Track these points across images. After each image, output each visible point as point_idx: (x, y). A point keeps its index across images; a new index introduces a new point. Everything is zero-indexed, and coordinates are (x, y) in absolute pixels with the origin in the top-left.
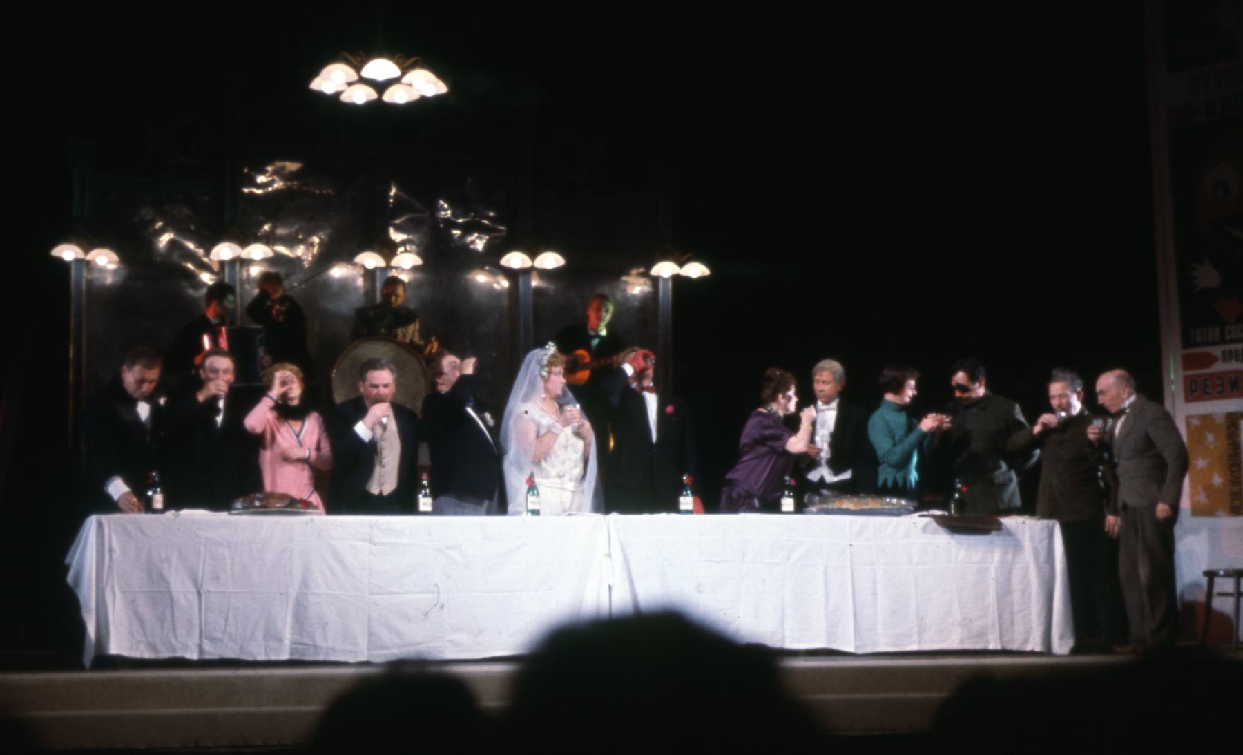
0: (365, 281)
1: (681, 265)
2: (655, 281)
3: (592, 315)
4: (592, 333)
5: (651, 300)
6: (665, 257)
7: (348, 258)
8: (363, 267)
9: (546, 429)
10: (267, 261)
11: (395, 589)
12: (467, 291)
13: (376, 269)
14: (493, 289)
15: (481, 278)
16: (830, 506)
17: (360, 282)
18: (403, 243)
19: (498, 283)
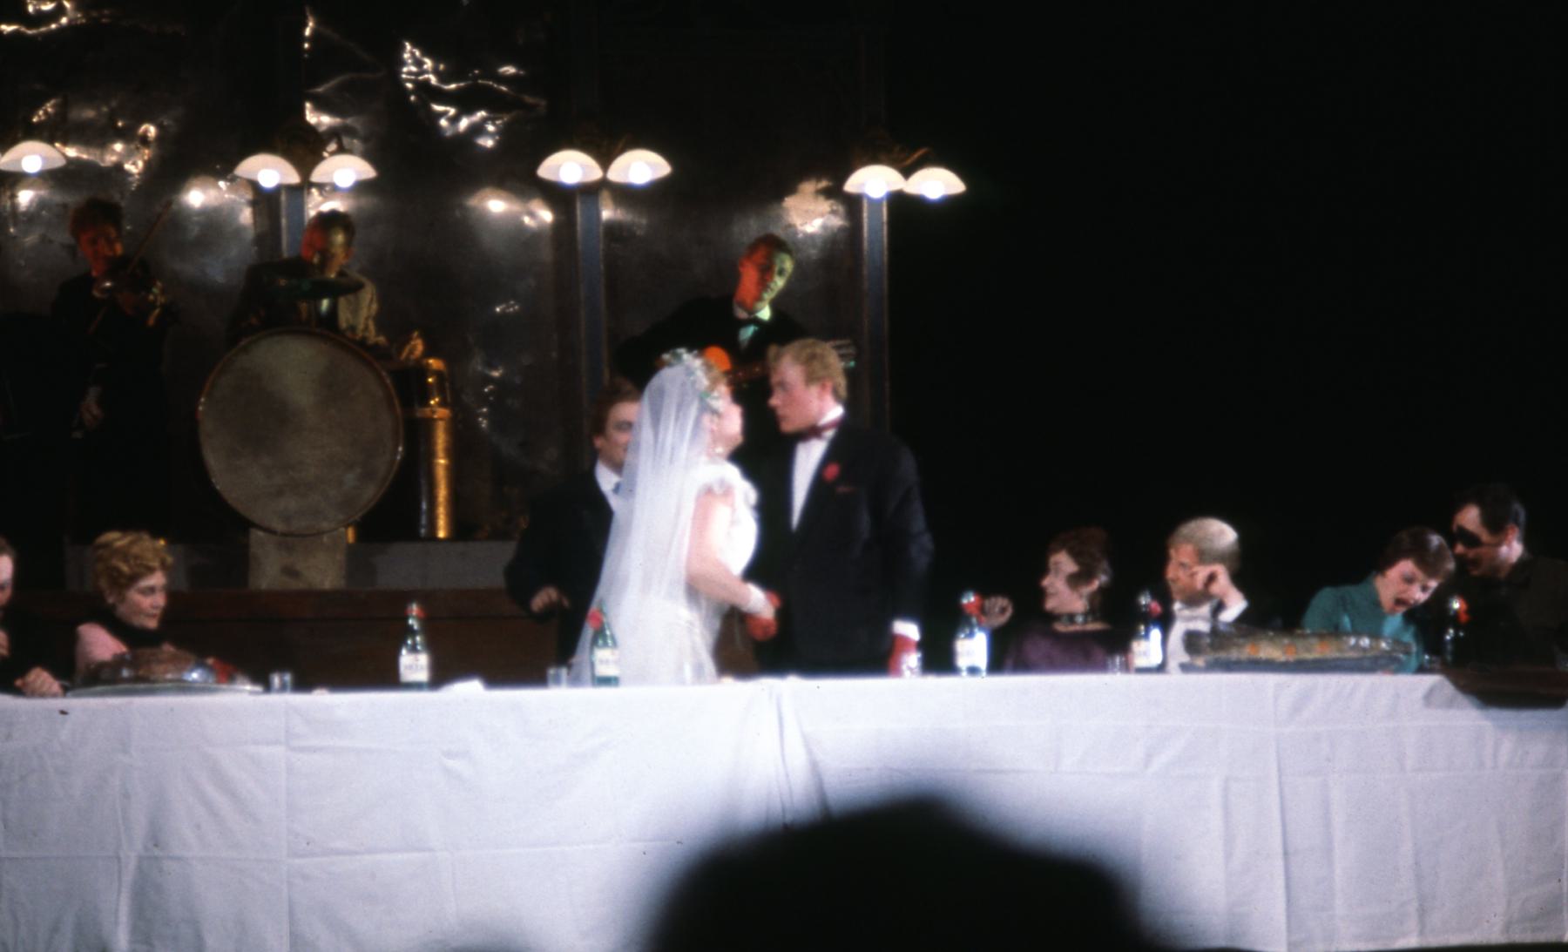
0: (255, 214)
1: (907, 172)
2: (853, 204)
4: (742, 314)
5: (842, 250)
7: (222, 165)
8: (254, 185)
9: (684, 502)
10: (51, 177)
11: (339, 844)
12: (466, 231)
13: (279, 189)
14: (521, 228)
15: (496, 205)
16: (1234, 654)
17: (246, 216)
18: (334, 133)
19: (532, 215)
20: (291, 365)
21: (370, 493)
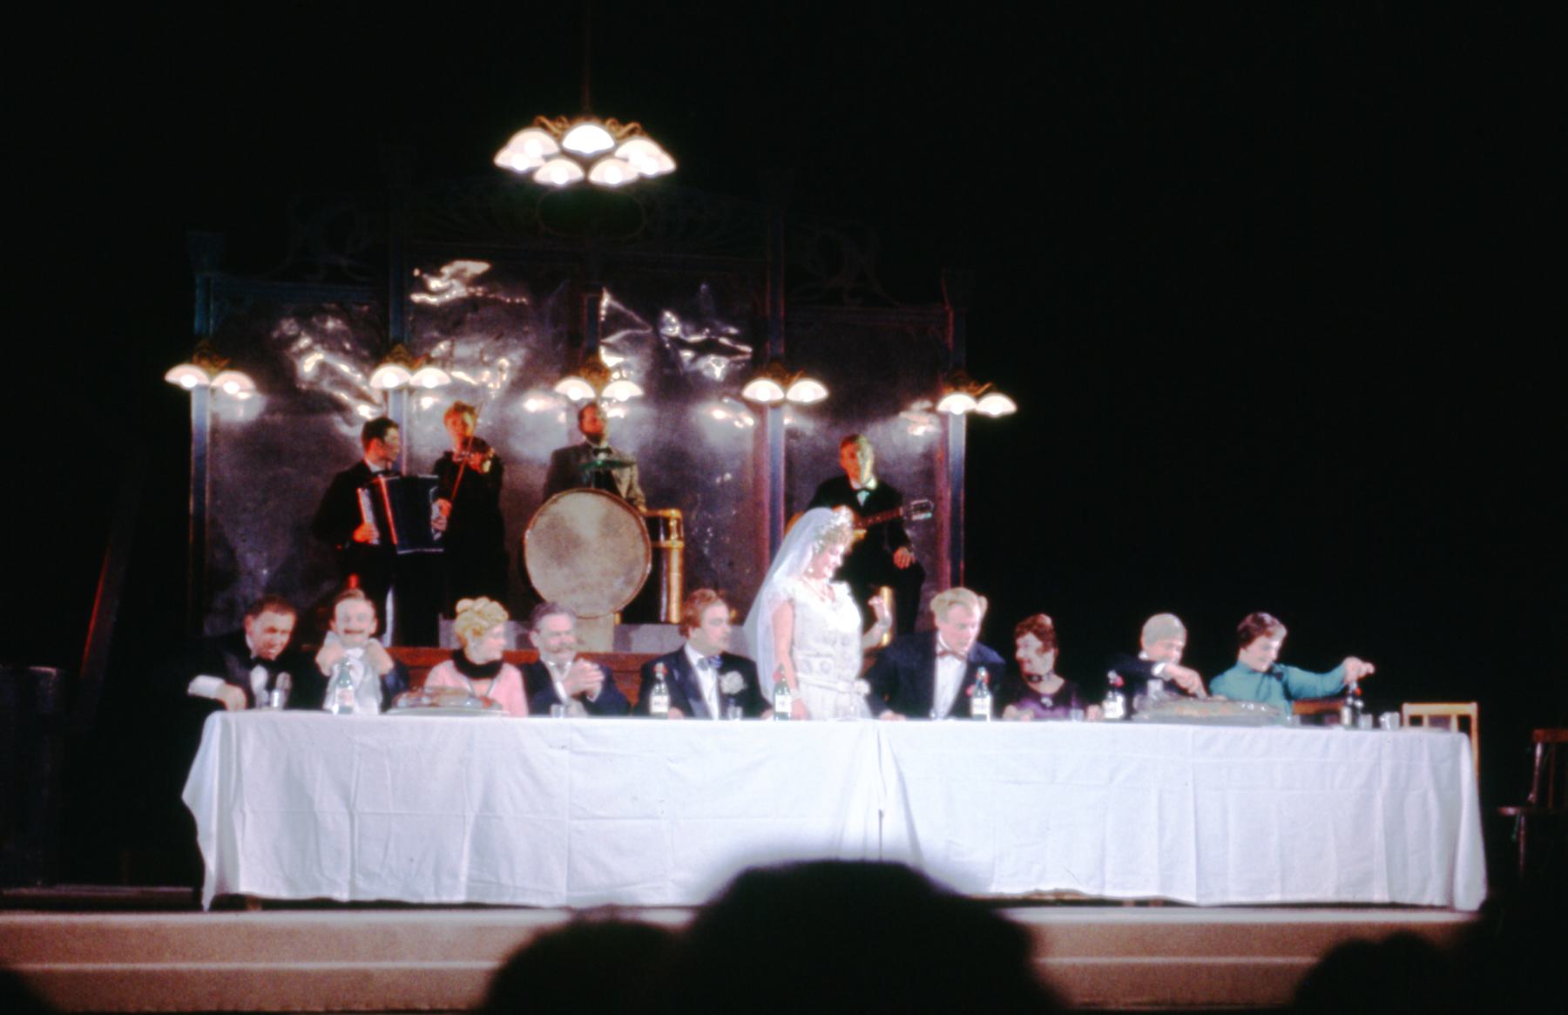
1: (978, 398)
2: (944, 418)
3: (847, 463)
6: (957, 385)
8: (566, 398)
18: (618, 368)
19: (740, 420)
20: (581, 510)
21: (629, 594)
